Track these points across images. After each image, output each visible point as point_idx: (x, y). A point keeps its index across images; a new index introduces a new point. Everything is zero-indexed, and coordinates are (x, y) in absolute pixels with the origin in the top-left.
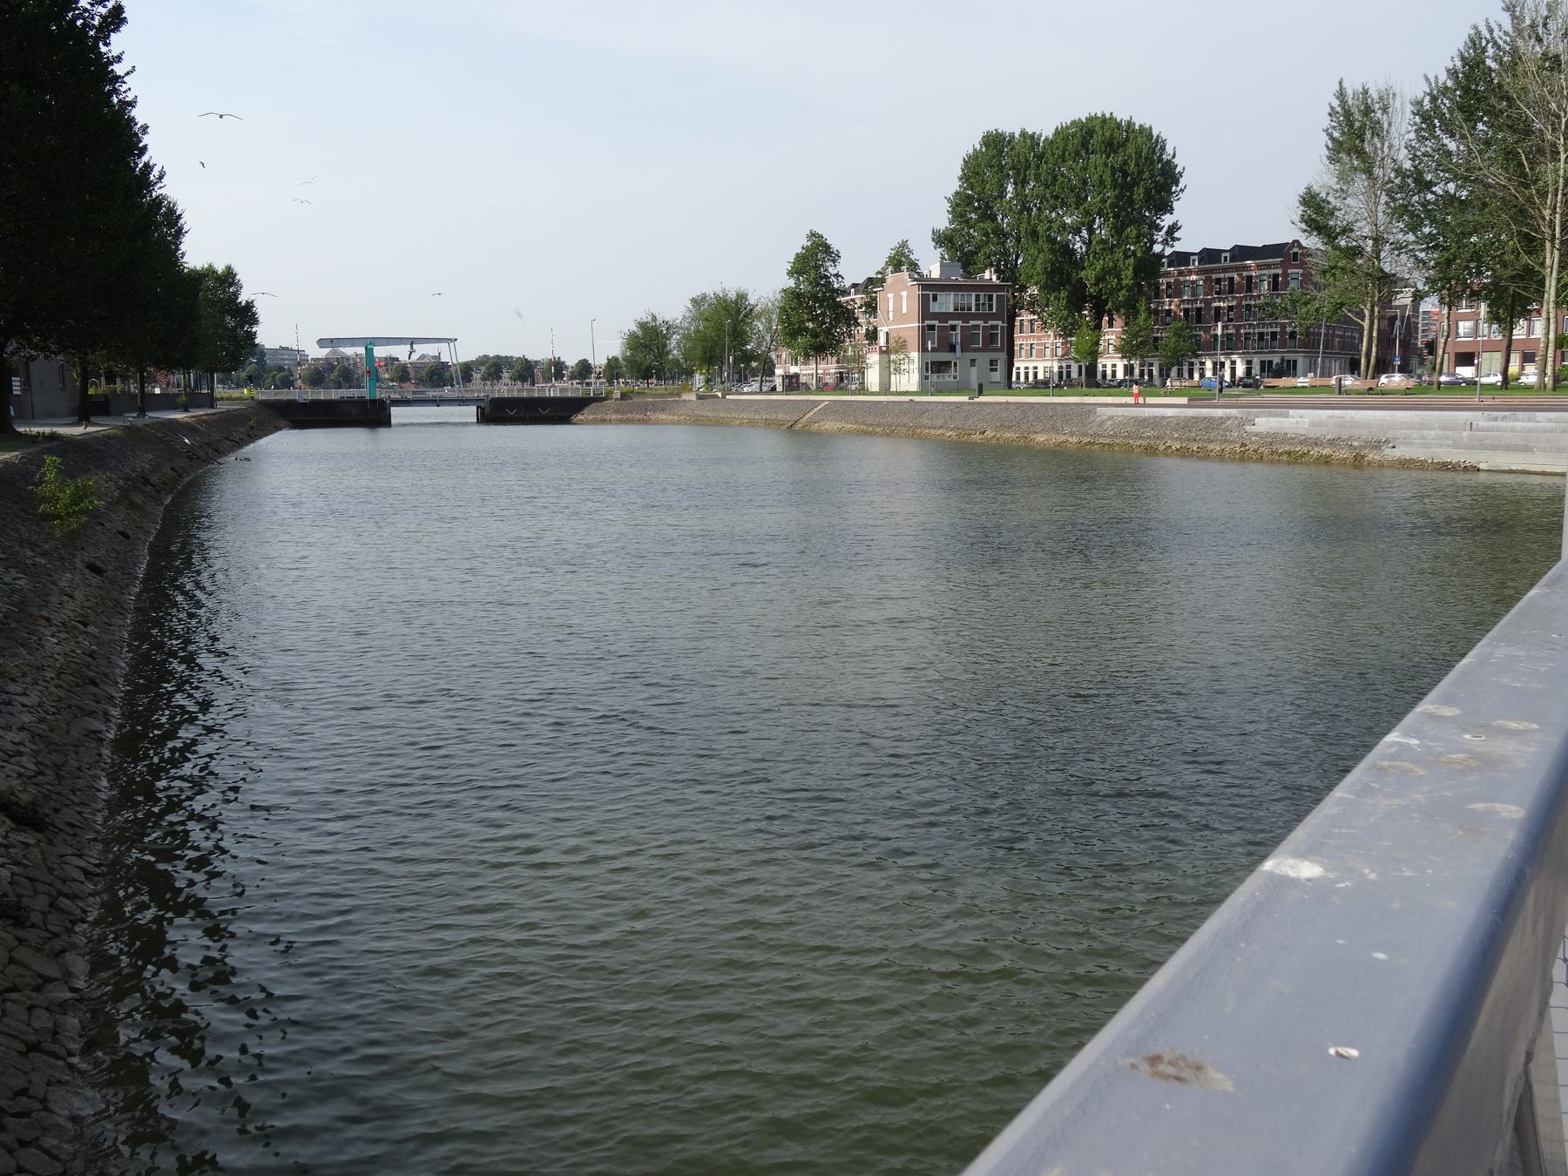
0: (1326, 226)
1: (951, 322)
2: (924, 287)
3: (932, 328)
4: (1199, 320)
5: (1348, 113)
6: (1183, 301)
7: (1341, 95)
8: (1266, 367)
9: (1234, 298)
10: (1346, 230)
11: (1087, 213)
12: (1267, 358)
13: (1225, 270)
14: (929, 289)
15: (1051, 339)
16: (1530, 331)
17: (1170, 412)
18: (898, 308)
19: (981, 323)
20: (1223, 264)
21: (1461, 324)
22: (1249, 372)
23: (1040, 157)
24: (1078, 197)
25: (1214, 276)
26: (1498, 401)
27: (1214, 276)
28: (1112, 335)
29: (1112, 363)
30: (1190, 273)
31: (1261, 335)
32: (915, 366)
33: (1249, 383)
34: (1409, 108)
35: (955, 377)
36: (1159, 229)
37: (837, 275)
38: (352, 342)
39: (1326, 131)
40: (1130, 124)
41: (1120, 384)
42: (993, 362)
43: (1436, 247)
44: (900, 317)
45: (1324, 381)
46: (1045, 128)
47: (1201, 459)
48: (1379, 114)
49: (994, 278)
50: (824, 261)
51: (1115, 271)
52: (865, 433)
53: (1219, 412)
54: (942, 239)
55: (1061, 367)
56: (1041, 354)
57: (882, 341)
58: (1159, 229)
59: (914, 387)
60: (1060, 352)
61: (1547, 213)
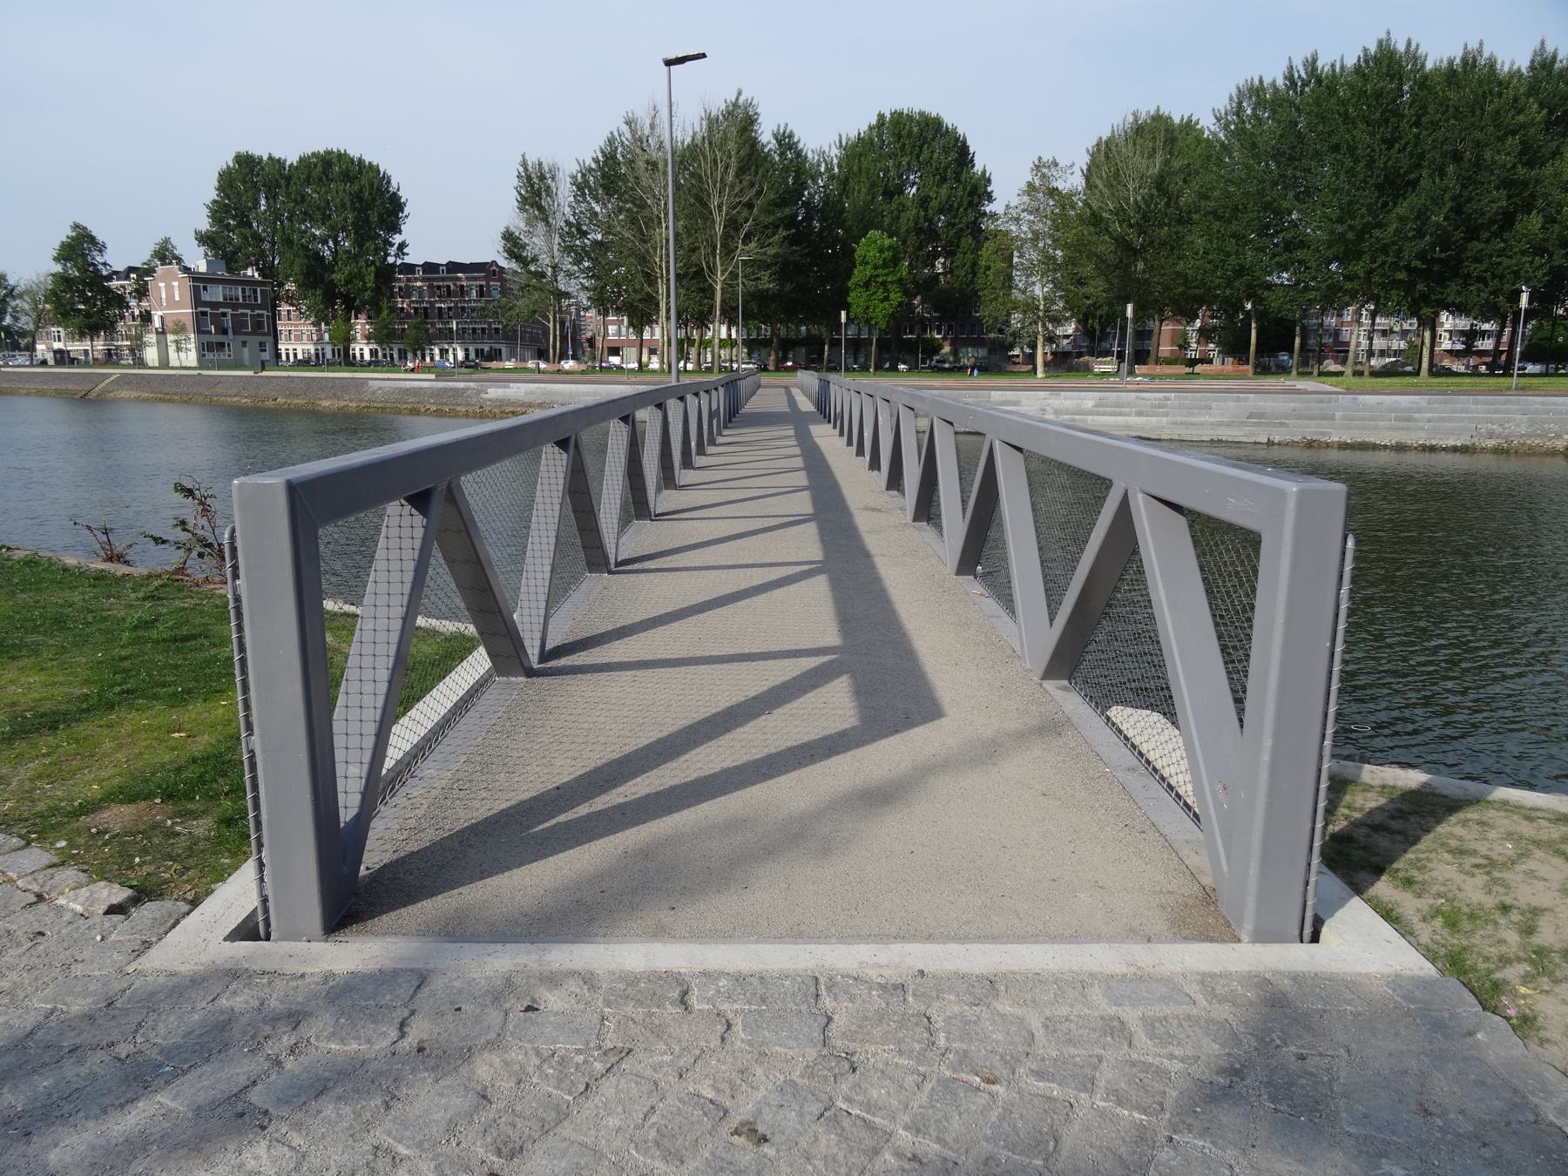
0: (521, 256)
1: (221, 310)
2: (195, 280)
3: (205, 314)
4: (426, 316)
5: (529, 178)
6: (413, 302)
7: (524, 164)
8: (479, 353)
9: (451, 301)
10: (535, 259)
11: (332, 228)
12: (480, 346)
13: (443, 279)
14: (199, 282)
15: (307, 328)
16: (652, 334)
17: (426, 384)
18: (170, 296)
19: (249, 312)
20: (441, 275)
21: (610, 327)
22: (467, 356)
23: (288, 179)
24: (324, 214)
25: (435, 284)
26: (638, 379)
27: (435, 284)
28: (361, 325)
29: (362, 349)
30: (416, 280)
31: (474, 330)
32: (192, 346)
33: (466, 364)
34: (569, 180)
35: (229, 356)
36: (392, 245)
37: (105, 264)
38: (1499, 375)
39: (516, 188)
40: (361, 161)
41: (370, 364)
42: (261, 344)
43: (592, 277)
44: (172, 303)
45: (522, 365)
46: (292, 158)
47: (454, 417)
48: (549, 181)
49: (256, 275)
50: (90, 250)
51: (360, 276)
52: (164, 401)
53: (462, 385)
54: (204, 239)
55: (317, 350)
56: (299, 338)
57: (157, 323)
58: (392, 245)
59: (194, 364)
60: (315, 337)
61: (657, 260)
